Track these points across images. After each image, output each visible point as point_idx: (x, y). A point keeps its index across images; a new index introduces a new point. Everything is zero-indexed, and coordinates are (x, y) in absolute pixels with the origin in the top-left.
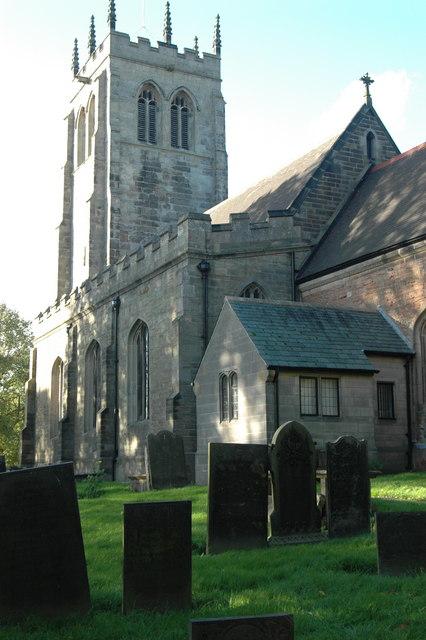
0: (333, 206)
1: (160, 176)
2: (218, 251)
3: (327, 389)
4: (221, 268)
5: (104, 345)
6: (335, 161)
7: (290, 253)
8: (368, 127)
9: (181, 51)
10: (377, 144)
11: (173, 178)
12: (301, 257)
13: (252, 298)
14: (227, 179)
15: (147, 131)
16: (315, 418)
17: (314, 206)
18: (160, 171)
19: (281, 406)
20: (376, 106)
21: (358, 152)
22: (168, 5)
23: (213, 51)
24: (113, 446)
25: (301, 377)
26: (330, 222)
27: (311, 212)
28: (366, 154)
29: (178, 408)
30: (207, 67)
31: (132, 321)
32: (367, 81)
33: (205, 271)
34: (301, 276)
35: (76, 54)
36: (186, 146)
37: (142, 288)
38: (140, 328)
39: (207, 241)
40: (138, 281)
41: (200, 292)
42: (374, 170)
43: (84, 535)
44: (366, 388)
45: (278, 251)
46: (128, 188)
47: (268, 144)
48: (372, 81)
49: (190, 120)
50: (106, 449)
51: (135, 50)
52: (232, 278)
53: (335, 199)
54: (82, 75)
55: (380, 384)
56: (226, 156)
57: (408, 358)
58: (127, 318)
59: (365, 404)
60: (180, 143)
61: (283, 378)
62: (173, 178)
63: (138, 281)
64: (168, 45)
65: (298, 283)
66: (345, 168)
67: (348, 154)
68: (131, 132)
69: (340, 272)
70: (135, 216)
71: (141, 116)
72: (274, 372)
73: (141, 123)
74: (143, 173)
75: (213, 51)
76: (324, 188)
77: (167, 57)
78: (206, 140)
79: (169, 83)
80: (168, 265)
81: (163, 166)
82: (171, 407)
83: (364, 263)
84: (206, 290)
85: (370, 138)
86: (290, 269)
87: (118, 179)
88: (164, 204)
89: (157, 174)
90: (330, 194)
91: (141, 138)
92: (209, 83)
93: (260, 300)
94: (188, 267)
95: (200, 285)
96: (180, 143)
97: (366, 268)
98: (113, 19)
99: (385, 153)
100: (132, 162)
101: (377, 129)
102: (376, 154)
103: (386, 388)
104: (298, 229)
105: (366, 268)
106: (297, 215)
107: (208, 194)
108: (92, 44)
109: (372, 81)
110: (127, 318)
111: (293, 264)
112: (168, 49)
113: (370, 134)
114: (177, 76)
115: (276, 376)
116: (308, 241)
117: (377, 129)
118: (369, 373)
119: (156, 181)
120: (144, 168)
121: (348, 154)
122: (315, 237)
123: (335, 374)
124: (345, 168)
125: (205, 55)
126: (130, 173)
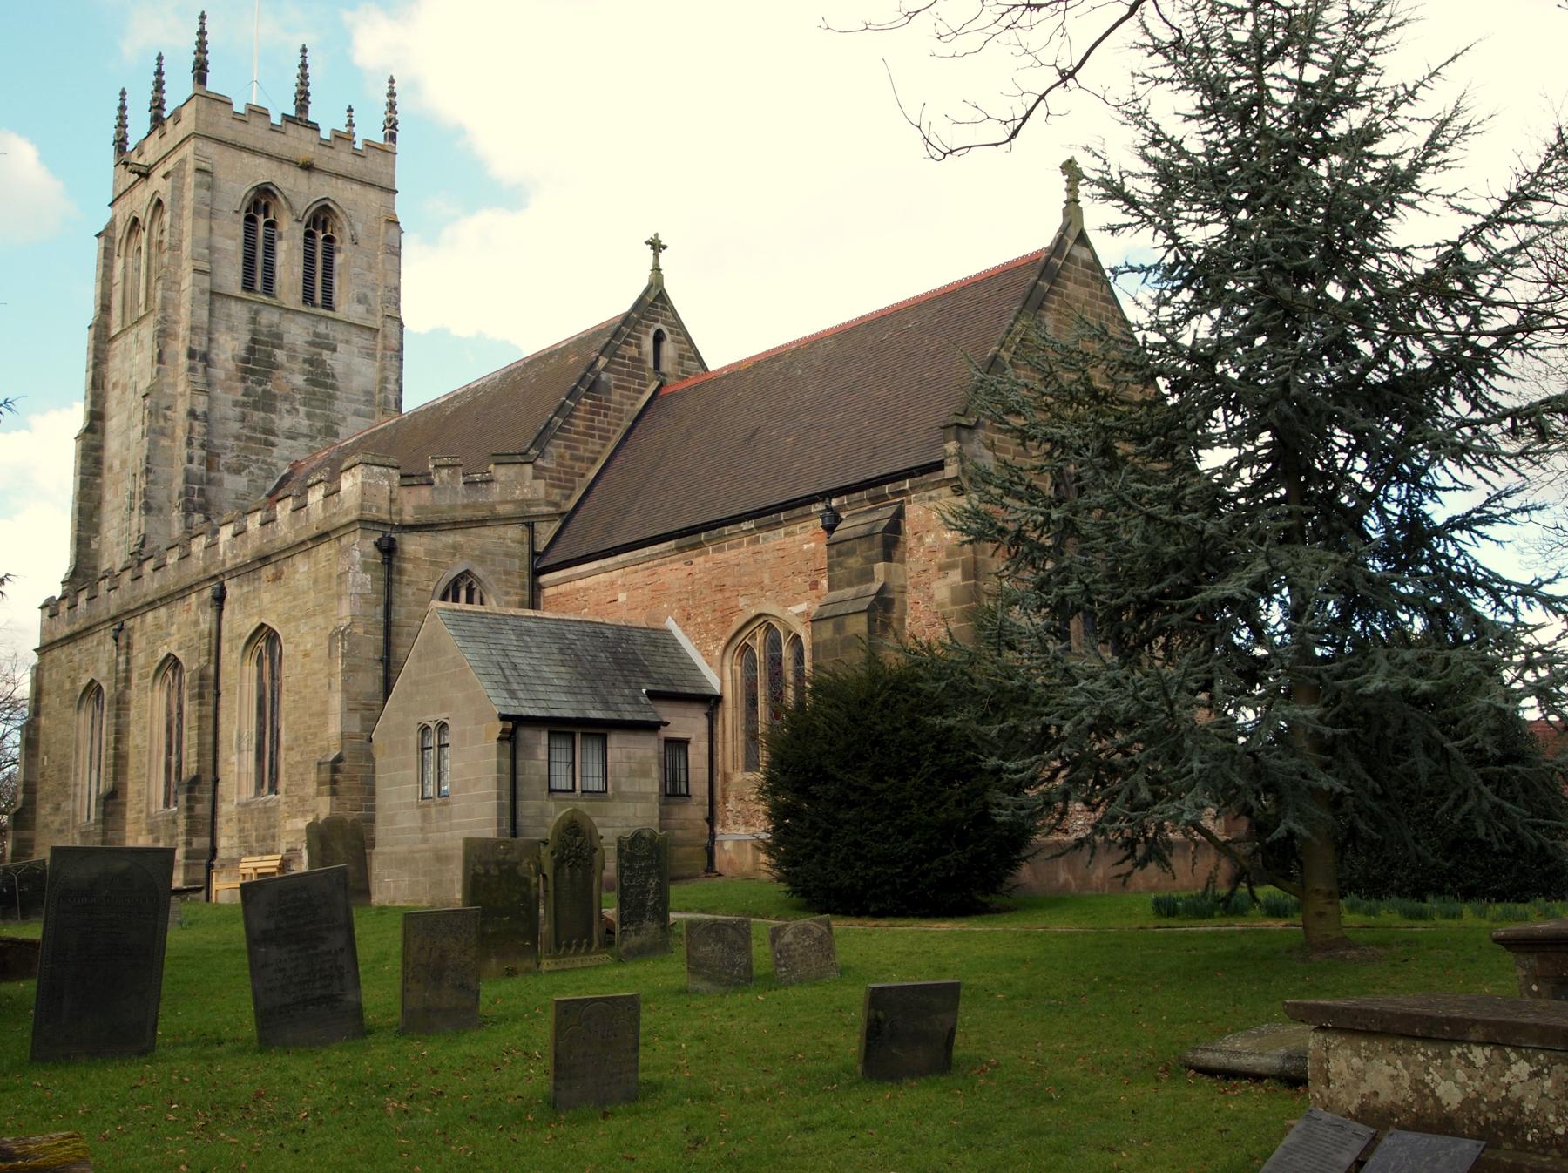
0: (597, 448)
1: (280, 356)
2: (408, 518)
3: (587, 755)
4: (413, 545)
5: (192, 664)
6: (604, 376)
7: (527, 525)
8: (656, 321)
9: (325, 134)
10: (668, 349)
11: (305, 361)
12: (546, 532)
13: (462, 605)
14: (401, 367)
15: (257, 271)
16: (570, 796)
17: (567, 447)
18: (280, 347)
19: (520, 777)
20: (670, 287)
21: (639, 361)
22: (350, 110)
23: (379, 138)
24: (207, 840)
25: (550, 733)
26: (591, 475)
27: (562, 456)
28: (651, 364)
29: (338, 777)
30: (374, 165)
31: (251, 625)
32: (656, 246)
33: (389, 550)
34: (539, 565)
35: (122, 118)
36: (328, 303)
37: (269, 571)
38: (265, 639)
39: (392, 501)
40: (264, 559)
41: (381, 585)
42: (664, 391)
43: (246, 961)
44: (647, 749)
45: (506, 520)
46: (222, 376)
47: (477, 303)
48: (665, 247)
49: (339, 259)
50: (195, 846)
51: (240, 126)
52: (432, 563)
53: (601, 438)
54: (134, 158)
55: (668, 741)
56: (401, 325)
57: (711, 702)
58: (239, 623)
59: (645, 774)
60: (318, 298)
61: (525, 734)
62: (305, 361)
63: (264, 559)
64: (300, 118)
65: (537, 573)
66: (617, 387)
67: (624, 365)
68: (231, 277)
69: (609, 561)
70: (235, 427)
71: (249, 243)
72: (510, 725)
73: (249, 260)
74: (251, 350)
75: (379, 138)
76: (584, 419)
77: (300, 144)
78: (366, 296)
79: (301, 191)
80: (321, 537)
81: (287, 339)
82: (326, 776)
83: (648, 551)
84: (389, 583)
85: (659, 338)
86: (526, 549)
87: (205, 357)
88: (288, 407)
89: (277, 352)
90: (593, 428)
91: (248, 285)
92: (373, 196)
93: (476, 607)
94: (361, 547)
95: (381, 574)
96: (318, 298)
97: (650, 558)
98: (201, 71)
99: (681, 364)
100: (230, 329)
101: (671, 325)
102: (666, 367)
103: (678, 746)
104: (541, 485)
105: (650, 558)
106: (540, 462)
107: (368, 393)
108: (158, 105)
109: (665, 247)
110: (239, 623)
111: (532, 543)
112: (302, 130)
113: (659, 332)
114: (316, 179)
115: (514, 731)
116: (556, 505)
117: (671, 325)
118: (652, 727)
119: (276, 366)
120: (254, 341)
121: (624, 365)
122: (568, 497)
123: (597, 730)
124: (617, 387)
125: (369, 145)
126: (229, 347)
